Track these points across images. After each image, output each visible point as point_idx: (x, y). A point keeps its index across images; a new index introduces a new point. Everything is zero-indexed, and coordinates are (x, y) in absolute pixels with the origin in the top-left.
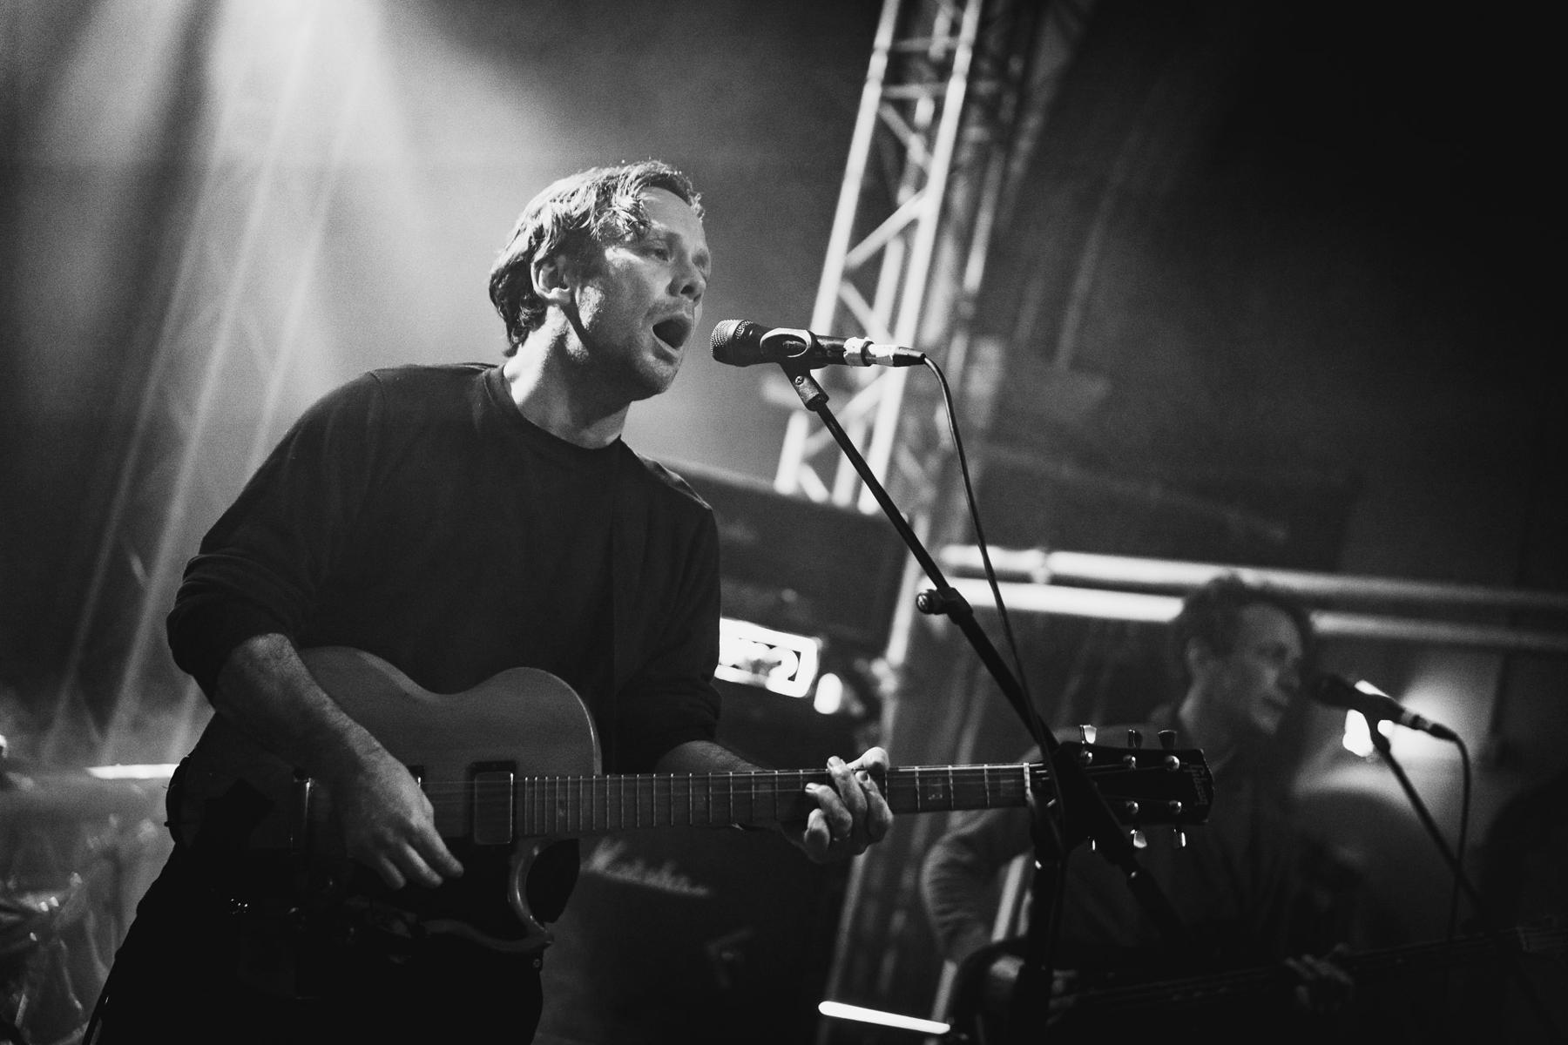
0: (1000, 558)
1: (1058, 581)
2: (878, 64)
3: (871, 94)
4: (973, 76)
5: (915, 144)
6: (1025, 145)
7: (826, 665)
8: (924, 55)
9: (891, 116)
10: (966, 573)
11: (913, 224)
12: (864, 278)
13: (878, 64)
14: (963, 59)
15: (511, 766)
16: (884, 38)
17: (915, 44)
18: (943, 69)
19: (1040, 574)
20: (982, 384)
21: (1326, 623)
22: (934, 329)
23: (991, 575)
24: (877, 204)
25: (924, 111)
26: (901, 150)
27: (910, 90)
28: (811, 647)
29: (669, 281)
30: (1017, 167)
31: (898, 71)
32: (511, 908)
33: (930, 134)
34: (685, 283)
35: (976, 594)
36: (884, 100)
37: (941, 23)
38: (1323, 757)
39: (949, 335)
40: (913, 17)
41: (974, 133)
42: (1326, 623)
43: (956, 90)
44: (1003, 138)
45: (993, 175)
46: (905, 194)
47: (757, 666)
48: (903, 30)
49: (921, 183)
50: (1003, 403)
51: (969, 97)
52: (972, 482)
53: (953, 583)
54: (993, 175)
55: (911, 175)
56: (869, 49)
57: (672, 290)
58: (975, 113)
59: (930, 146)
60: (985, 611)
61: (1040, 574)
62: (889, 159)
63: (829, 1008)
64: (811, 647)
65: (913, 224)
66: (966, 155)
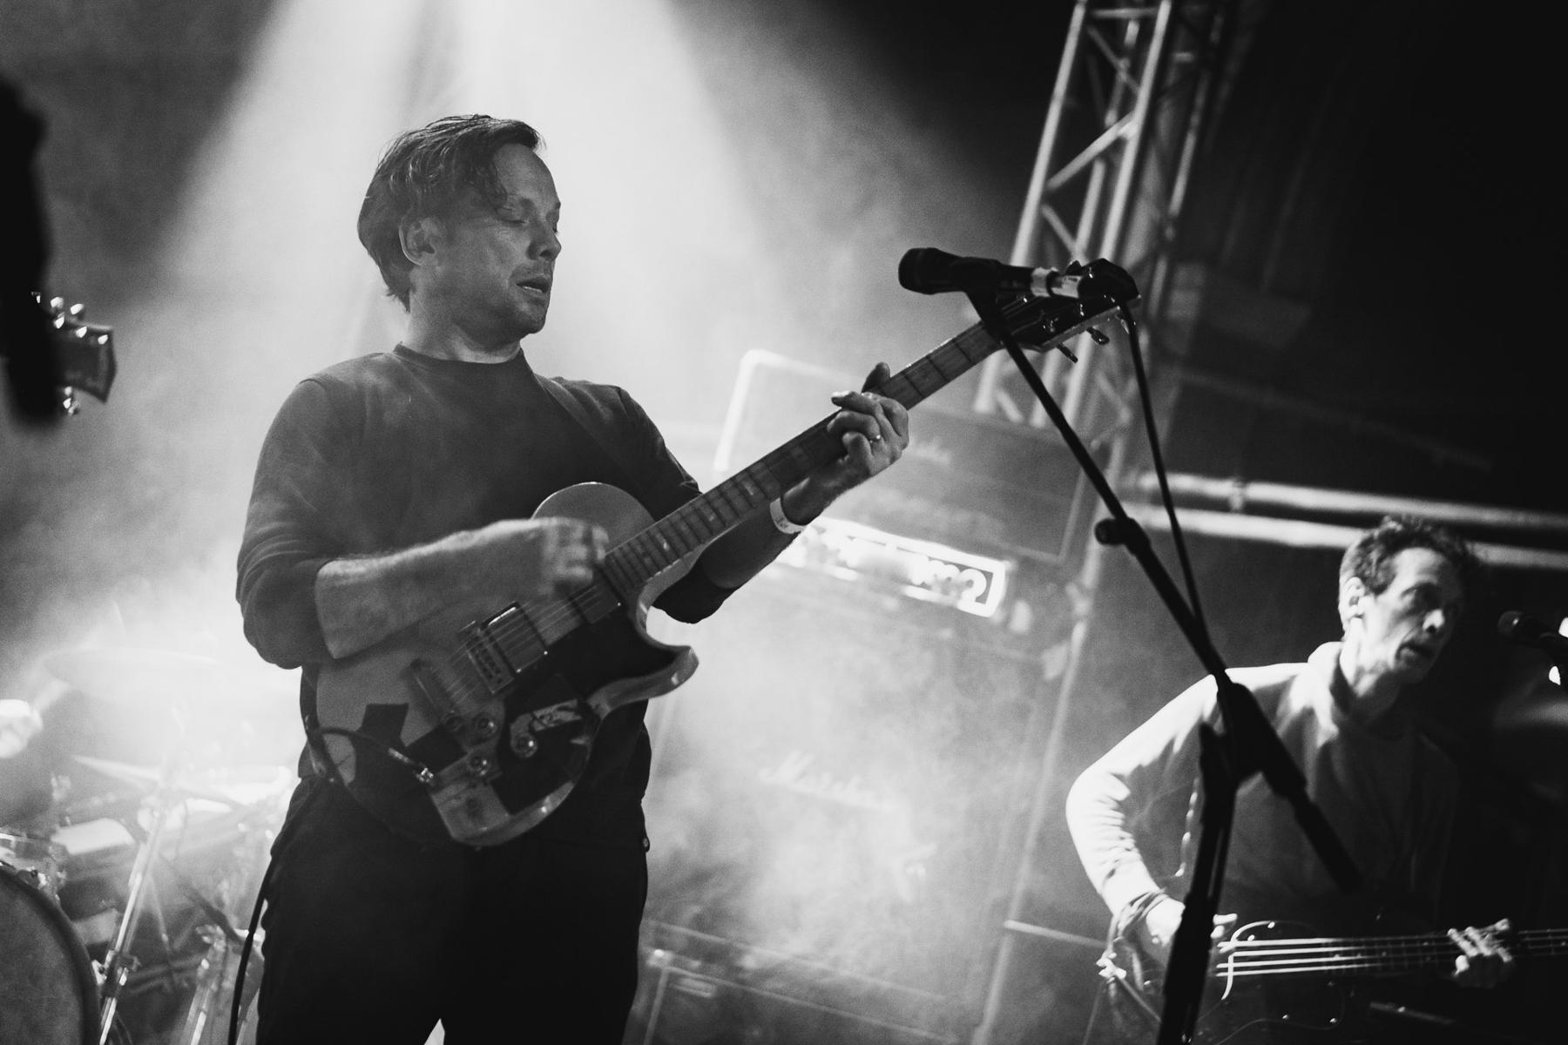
0: (1182, 483)
1: (1255, 509)
7: (1016, 590)
9: (1094, 34)
10: (1138, 496)
11: (1118, 144)
12: (1066, 200)
19: (1237, 502)
20: (1184, 305)
21: (1493, 554)
22: (1135, 252)
23: (1168, 500)
24: (1081, 127)
26: (1109, 73)
28: (1000, 569)
29: (527, 243)
30: (1225, 91)
34: (543, 249)
35: (1154, 519)
36: (1088, 20)
39: (1151, 258)
42: (1493, 554)
44: (1211, 60)
47: (947, 585)
50: (1203, 329)
53: (1131, 511)
57: (531, 252)
58: (1182, 34)
59: (1136, 72)
60: (1160, 534)
61: (1237, 502)
62: (1094, 74)
63: (1374, 1005)
64: (1000, 569)
65: (1118, 144)
66: (1172, 78)
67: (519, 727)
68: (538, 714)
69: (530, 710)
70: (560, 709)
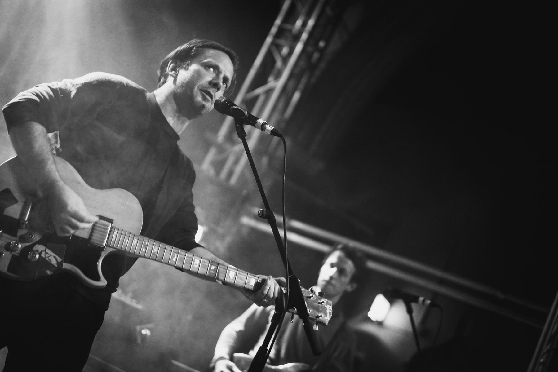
2: (274, 30)
3: (269, 40)
4: (306, 44)
5: (279, 64)
6: (317, 73)
8: (290, 31)
13: (274, 30)
14: (304, 36)
15: (111, 221)
16: (278, 22)
17: (288, 26)
18: (296, 38)
21: (371, 265)
24: (261, 79)
25: (285, 51)
26: (274, 62)
27: (281, 42)
30: (313, 80)
31: (278, 36)
32: (96, 266)
33: (285, 60)
37: (299, 23)
38: (361, 316)
40: (290, 17)
41: (329, 11)
42: (371, 265)
43: (299, 47)
45: (304, 80)
46: (271, 79)
48: (285, 21)
49: (278, 76)
51: (303, 51)
52: (266, 191)
54: (304, 80)
55: (275, 71)
56: (272, 24)
57: (210, 83)
66: (297, 71)
67: (40, 248)
68: (48, 251)
69: (47, 247)
70: (55, 257)
